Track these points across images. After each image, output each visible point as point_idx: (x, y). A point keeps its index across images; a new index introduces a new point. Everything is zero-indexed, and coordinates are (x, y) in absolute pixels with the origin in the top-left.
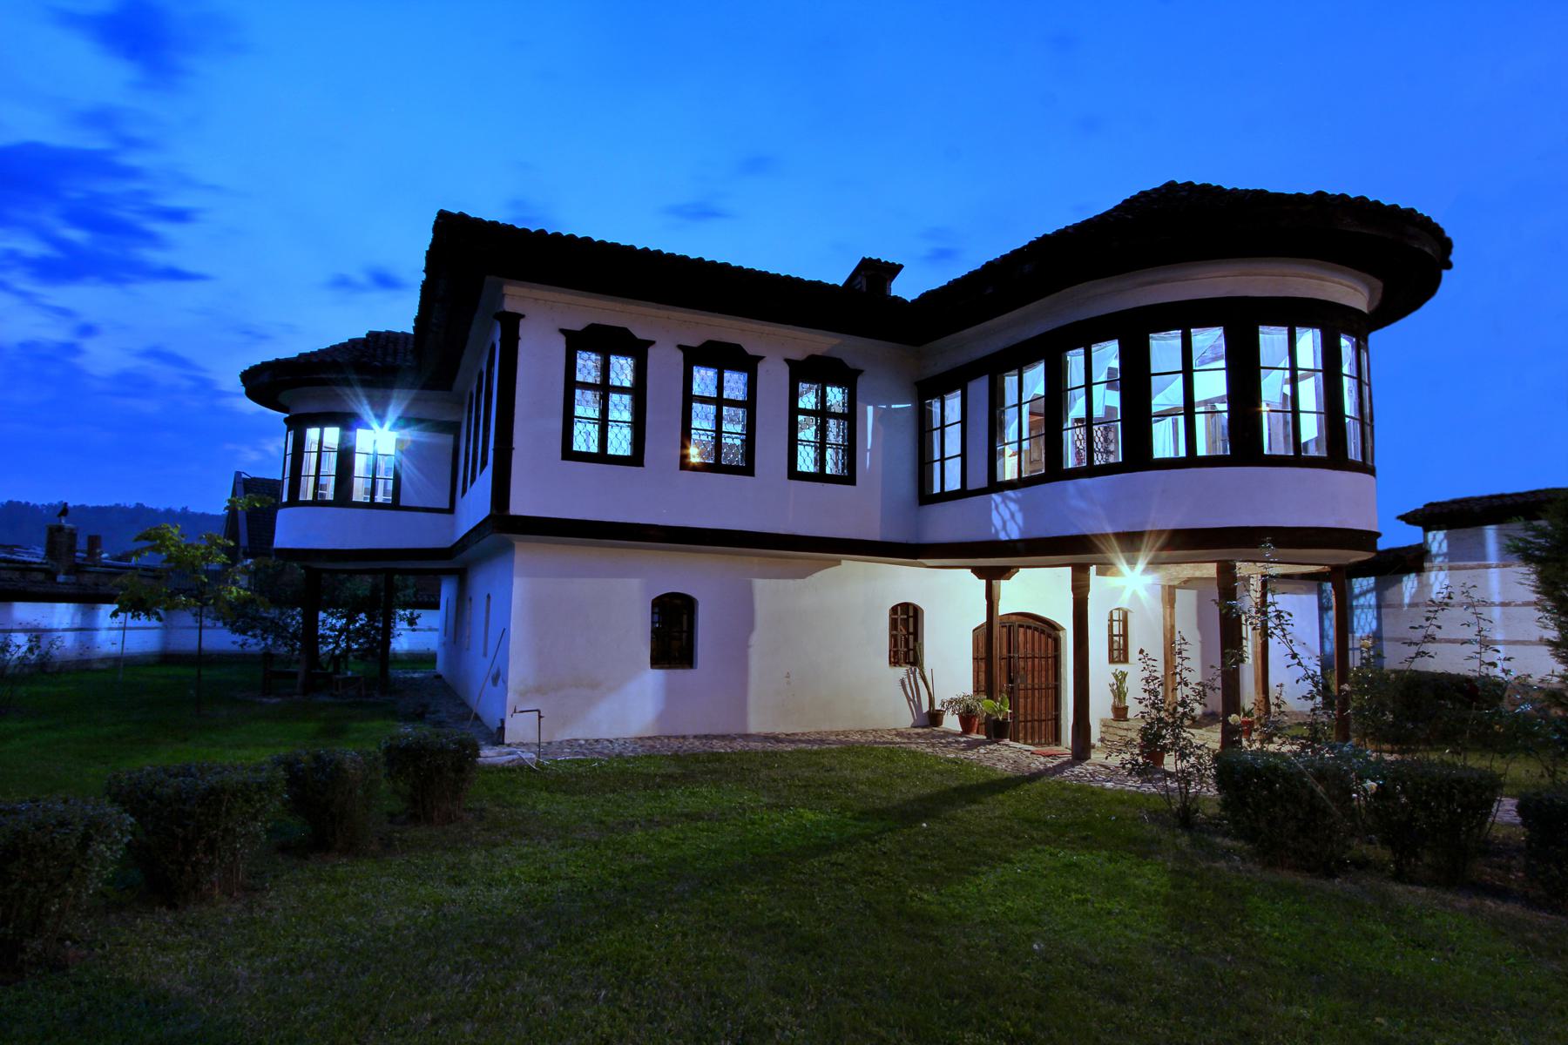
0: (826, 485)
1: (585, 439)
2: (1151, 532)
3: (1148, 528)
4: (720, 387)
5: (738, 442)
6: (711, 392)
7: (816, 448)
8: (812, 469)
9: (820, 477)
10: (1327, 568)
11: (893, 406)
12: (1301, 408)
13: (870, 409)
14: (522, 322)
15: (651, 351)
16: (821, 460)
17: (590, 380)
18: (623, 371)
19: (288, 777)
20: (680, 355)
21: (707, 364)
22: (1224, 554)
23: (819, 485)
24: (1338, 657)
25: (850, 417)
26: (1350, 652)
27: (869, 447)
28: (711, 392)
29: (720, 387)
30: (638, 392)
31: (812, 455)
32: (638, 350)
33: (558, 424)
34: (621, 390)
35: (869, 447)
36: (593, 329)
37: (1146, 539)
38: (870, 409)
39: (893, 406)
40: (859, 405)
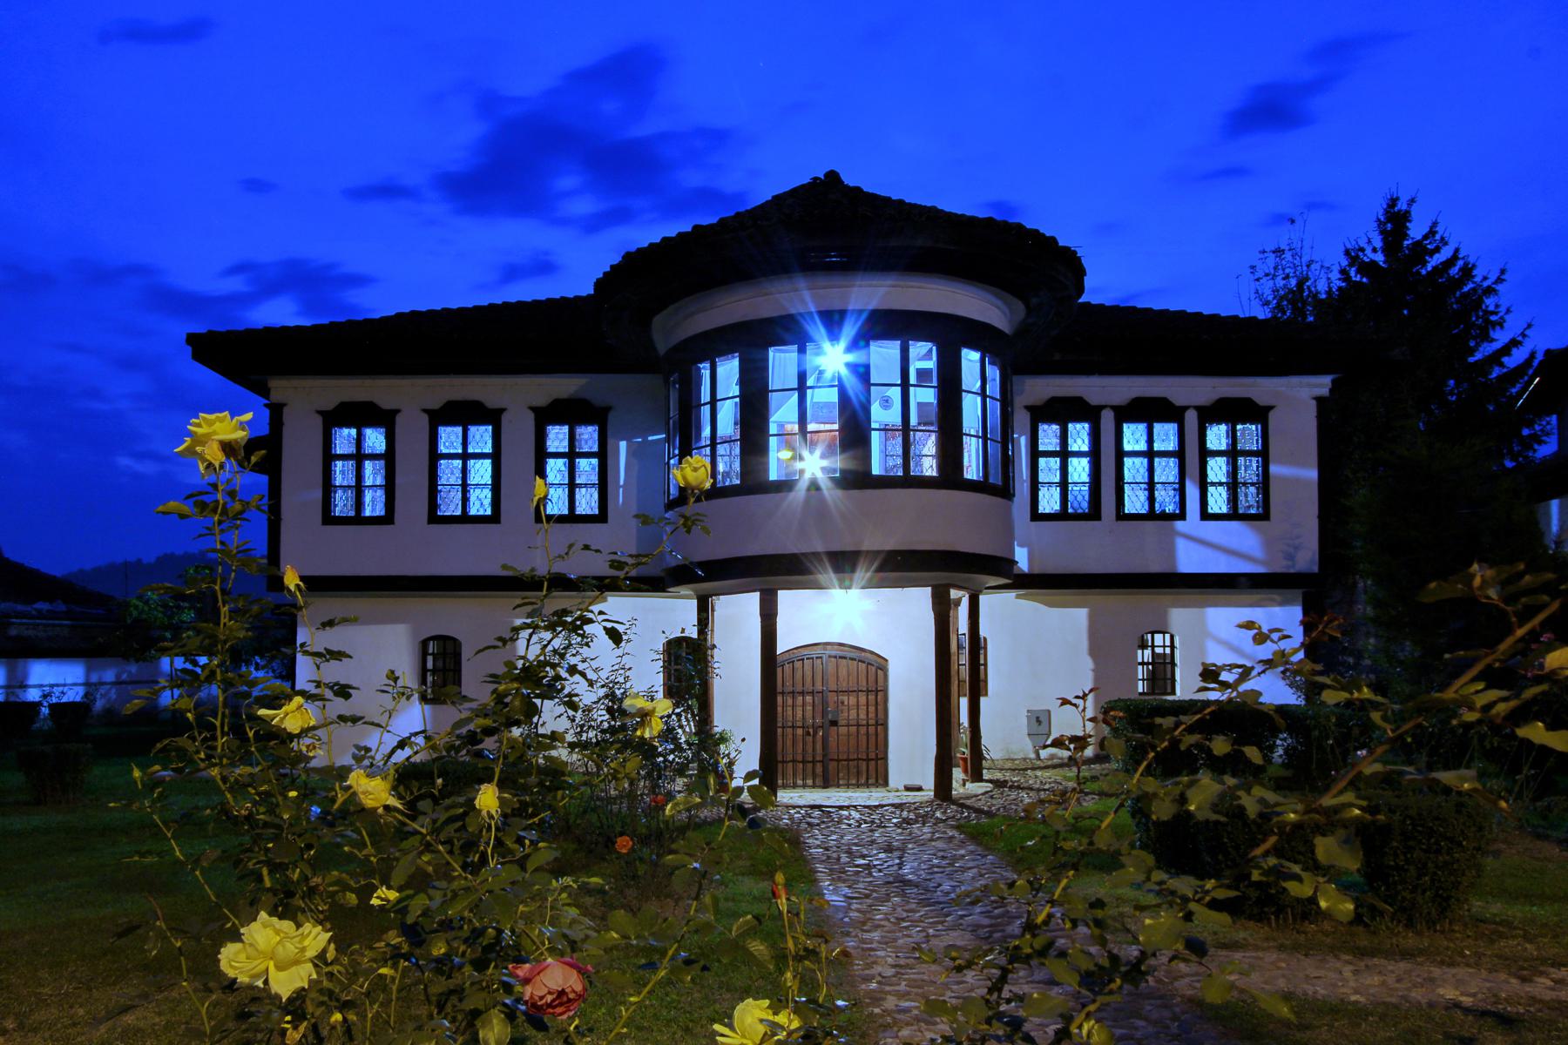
0: (574, 525)
1: (342, 504)
2: (868, 552)
3: (865, 547)
4: (1150, 441)
5: (1087, 488)
6: (1142, 446)
7: (1228, 489)
8: (1224, 510)
9: (358, 519)
10: (670, 590)
11: (650, 438)
12: (899, 388)
13: (623, 445)
14: (286, 410)
15: (399, 419)
16: (1233, 499)
17: (1051, 448)
18: (482, 439)
19: (717, 1027)
20: (425, 418)
21: (1050, 420)
22: (942, 577)
23: (567, 526)
24: (777, 772)
25: (603, 455)
26: (780, 766)
27: (622, 483)
28: (1142, 446)
29: (1150, 441)
30: (389, 457)
31: (1225, 495)
32: (385, 419)
33: (318, 494)
34: (1079, 454)
35: (622, 483)
36: (557, 403)
37: (862, 560)
38: (623, 445)
39: (650, 438)
40: (611, 442)
